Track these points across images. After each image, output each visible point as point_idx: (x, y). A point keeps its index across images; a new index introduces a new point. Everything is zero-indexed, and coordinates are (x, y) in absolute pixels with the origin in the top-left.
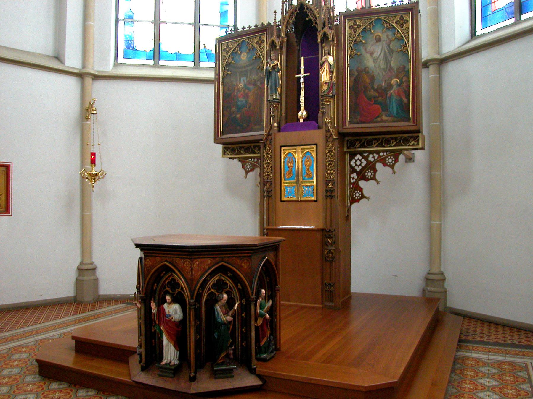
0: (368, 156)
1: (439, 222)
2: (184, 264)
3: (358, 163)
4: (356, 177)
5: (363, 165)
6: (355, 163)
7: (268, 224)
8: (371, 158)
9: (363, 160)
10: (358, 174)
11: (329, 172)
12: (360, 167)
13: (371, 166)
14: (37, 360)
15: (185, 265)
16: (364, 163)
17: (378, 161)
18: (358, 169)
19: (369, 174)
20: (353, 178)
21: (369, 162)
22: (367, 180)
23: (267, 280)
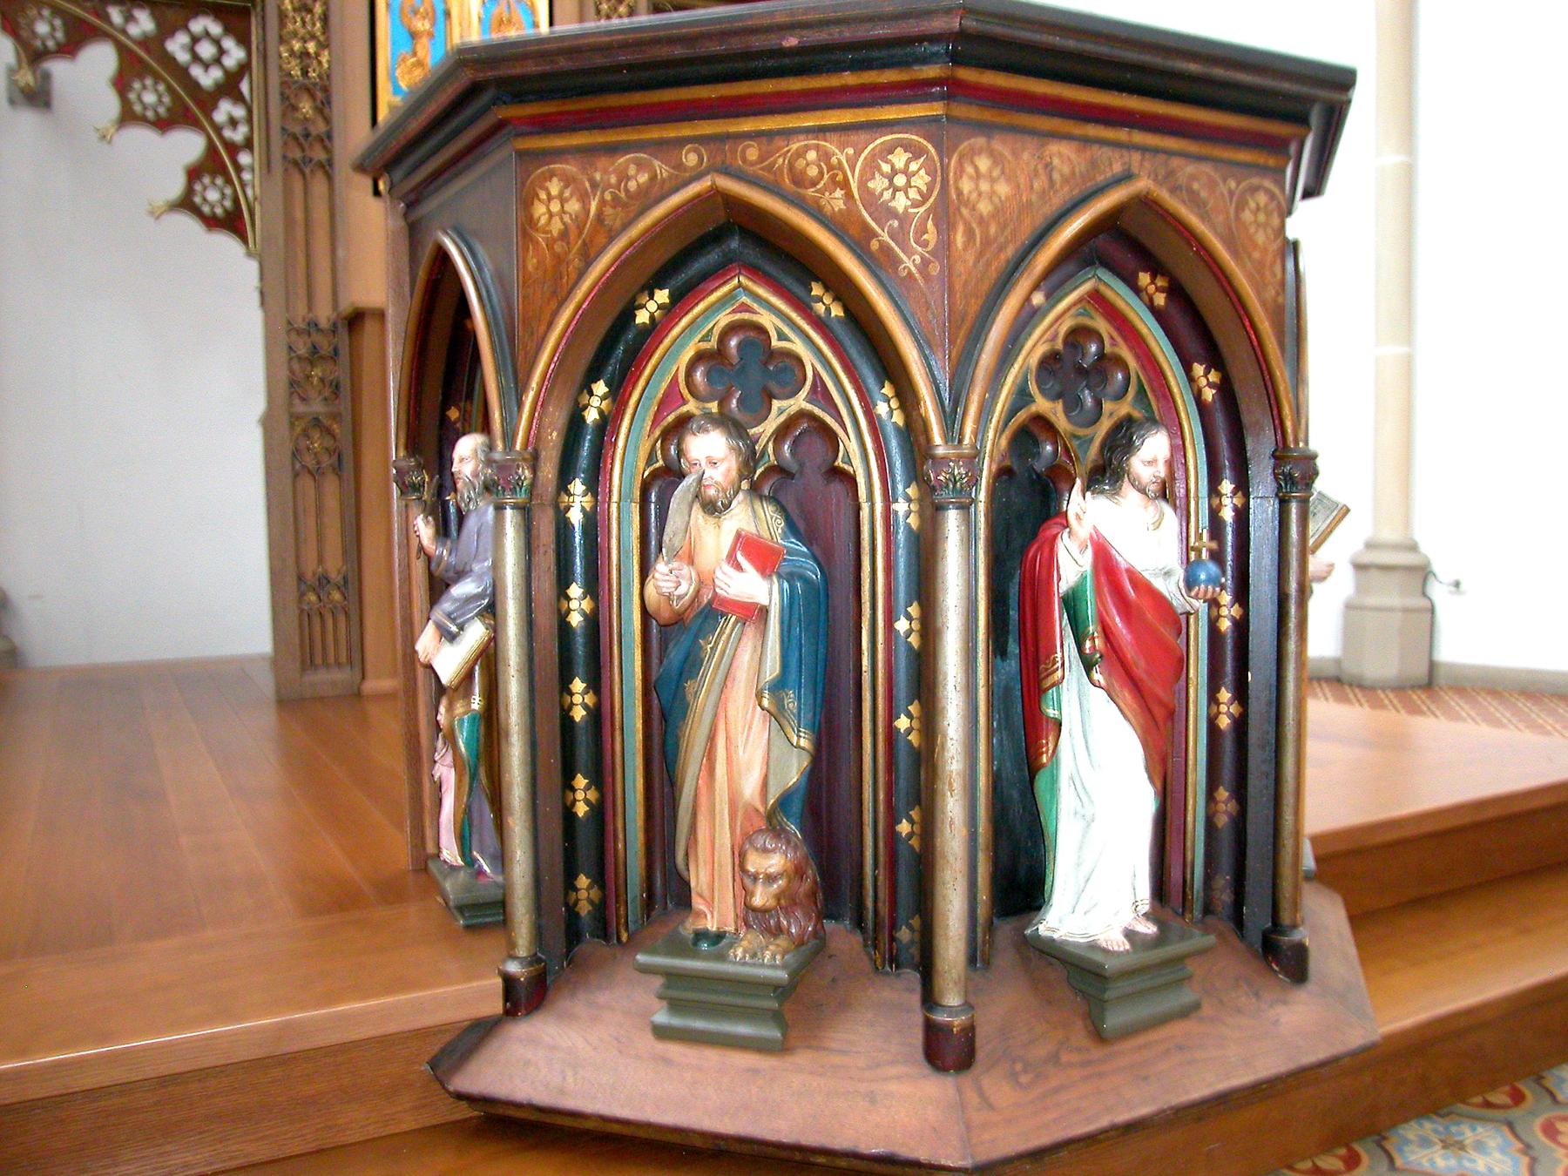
0: (238, 98)
1: (1403, 350)
2: (1241, 206)
3: (206, 50)
4: (134, 30)
5: (196, 71)
6: (207, 34)
7: (551, 24)
8: (225, 109)
9: (216, 74)
10: (154, 44)
11: (297, 46)
12: (183, 57)
13: (188, 108)
14: (1332, 566)
15: (1247, 216)
16: (207, 79)
17: (122, 49)
18: (177, 46)
19: (150, 96)
20: (233, 123)
21: (208, 100)
22: (121, 84)
23: (412, 197)
